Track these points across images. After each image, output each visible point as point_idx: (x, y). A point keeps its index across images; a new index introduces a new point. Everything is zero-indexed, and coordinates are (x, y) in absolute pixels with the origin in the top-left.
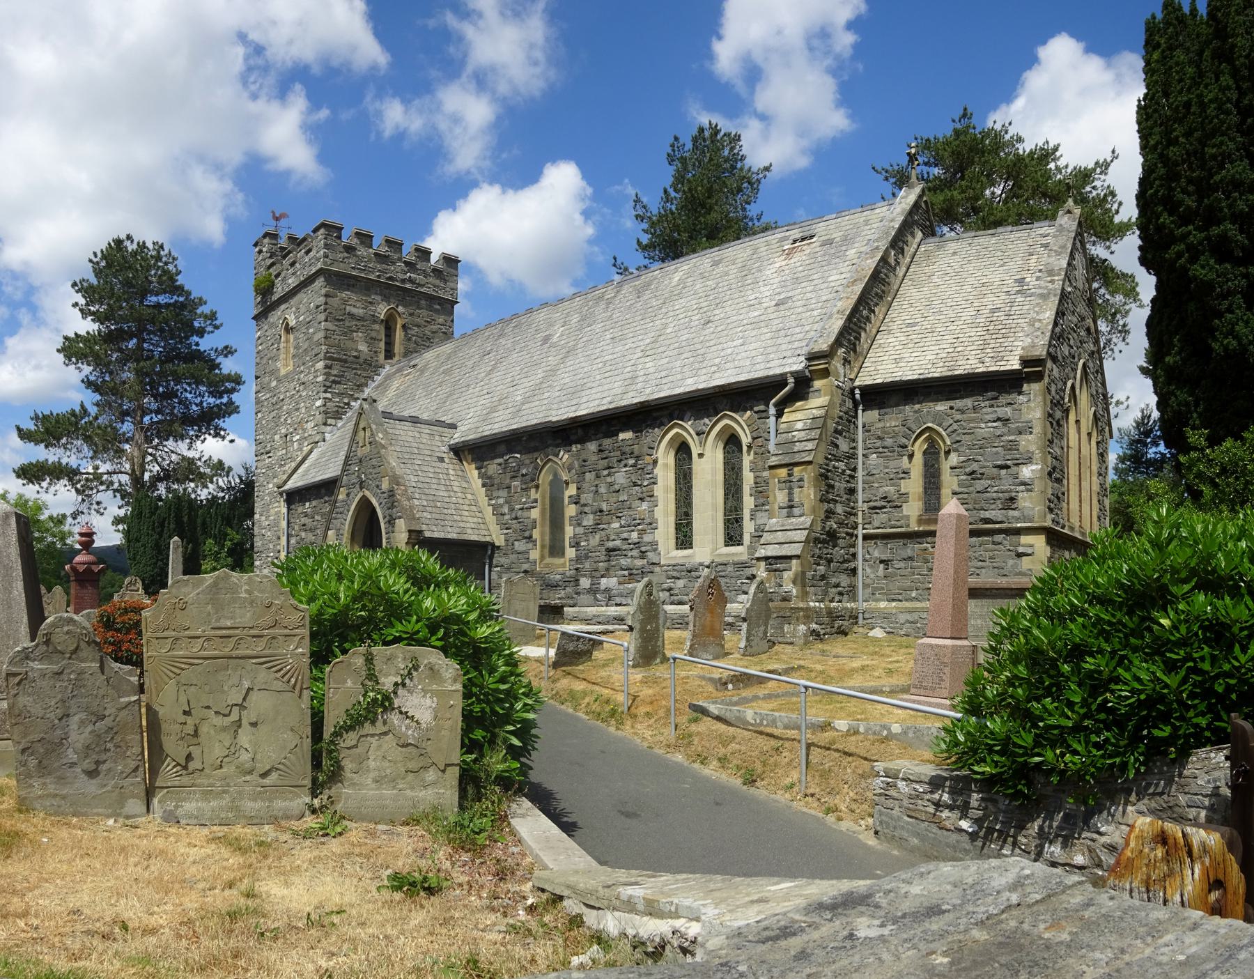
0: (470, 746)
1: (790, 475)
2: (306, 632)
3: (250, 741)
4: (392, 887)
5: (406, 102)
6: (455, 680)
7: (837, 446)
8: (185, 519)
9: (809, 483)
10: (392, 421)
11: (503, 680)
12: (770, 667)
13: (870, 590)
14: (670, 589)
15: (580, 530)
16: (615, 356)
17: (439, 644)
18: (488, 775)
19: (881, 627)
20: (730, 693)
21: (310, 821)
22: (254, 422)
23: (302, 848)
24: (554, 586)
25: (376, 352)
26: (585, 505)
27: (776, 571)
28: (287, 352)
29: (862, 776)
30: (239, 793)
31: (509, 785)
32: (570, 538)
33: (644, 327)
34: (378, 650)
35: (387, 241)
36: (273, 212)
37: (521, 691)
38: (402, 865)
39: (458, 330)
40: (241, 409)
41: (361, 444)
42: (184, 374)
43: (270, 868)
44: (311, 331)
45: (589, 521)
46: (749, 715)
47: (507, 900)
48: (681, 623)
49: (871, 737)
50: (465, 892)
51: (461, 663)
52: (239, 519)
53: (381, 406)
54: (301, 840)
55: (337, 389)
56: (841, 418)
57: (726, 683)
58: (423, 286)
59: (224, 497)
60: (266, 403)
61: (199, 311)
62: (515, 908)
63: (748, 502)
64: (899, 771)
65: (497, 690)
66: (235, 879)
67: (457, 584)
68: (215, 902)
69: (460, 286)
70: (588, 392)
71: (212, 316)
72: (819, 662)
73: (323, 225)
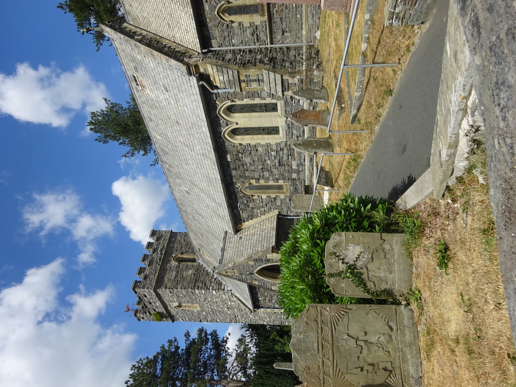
0: (371, 228)
1: (244, 81)
2: (319, 306)
3: (374, 336)
4: (445, 267)
5: (80, 252)
6: (340, 235)
7: (230, 59)
8: (265, 360)
9: (247, 72)
10: (223, 260)
11: (340, 213)
12: (334, 87)
13: (297, 40)
14: (298, 137)
15: (271, 178)
16: (194, 163)
17: (323, 242)
18: (386, 219)
19: (315, 33)
20: (346, 106)
21: (414, 306)
22: (221, 323)
23: (429, 311)
24: (296, 189)
25: (193, 266)
26: (260, 176)
27: (288, 87)
28: (190, 307)
29: (391, 33)
30: (402, 343)
31: (389, 211)
32: (274, 182)
33: (181, 151)
34: (327, 271)
35: (143, 261)
36: (126, 311)
37: (345, 204)
38: (433, 262)
39: (184, 230)
40: (214, 329)
41: (233, 274)
42: (196, 357)
43: (441, 329)
44: (181, 295)
45: (266, 174)
46: (357, 94)
47: (450, 212)
48: (313, 130)
49: (371, 30)
50: (446, 232)
51: (332, 232)
52: (266, 332)
53: (217, 264)
54: (424, 311)
55: (208, 284)
56: (216, 58)
57: (342, 108)
58: (164, 246)
59: (256, 339)
60: (213, 317)
61: (167, 348)
62: (454, 208)
63: (257, 101)
64: (390, 11)
65: (345, 215)
66: (449, 349)
67: (296, 233)
68: (464, 361)
69: (164, 229)
70: (210, 175)
71: (170, 342)
72: (332, 63)
73: (134, 289)
